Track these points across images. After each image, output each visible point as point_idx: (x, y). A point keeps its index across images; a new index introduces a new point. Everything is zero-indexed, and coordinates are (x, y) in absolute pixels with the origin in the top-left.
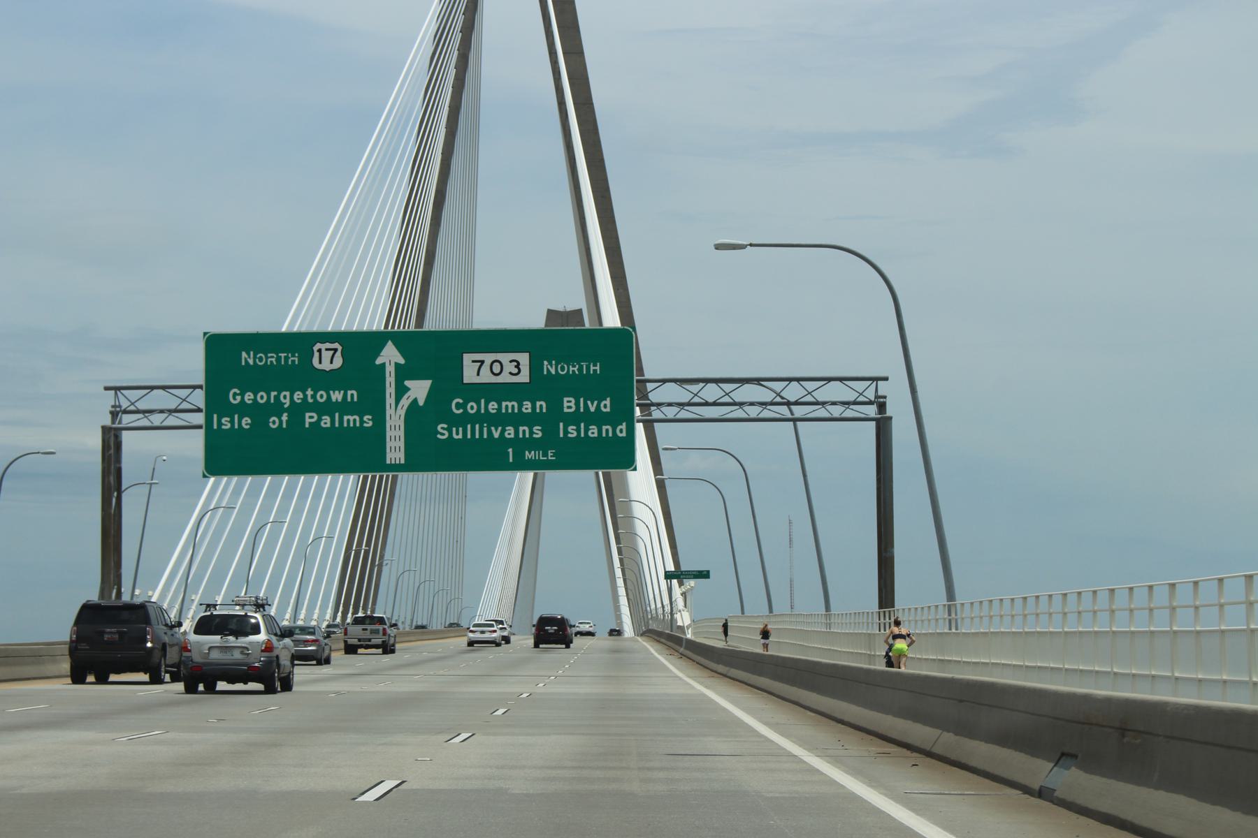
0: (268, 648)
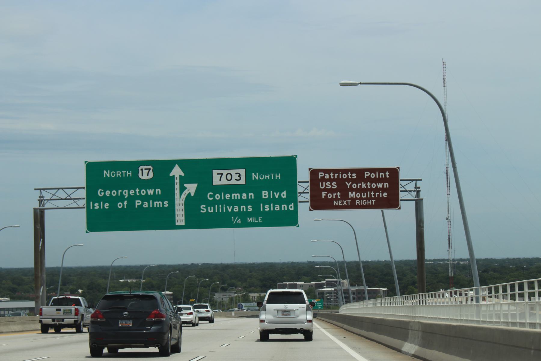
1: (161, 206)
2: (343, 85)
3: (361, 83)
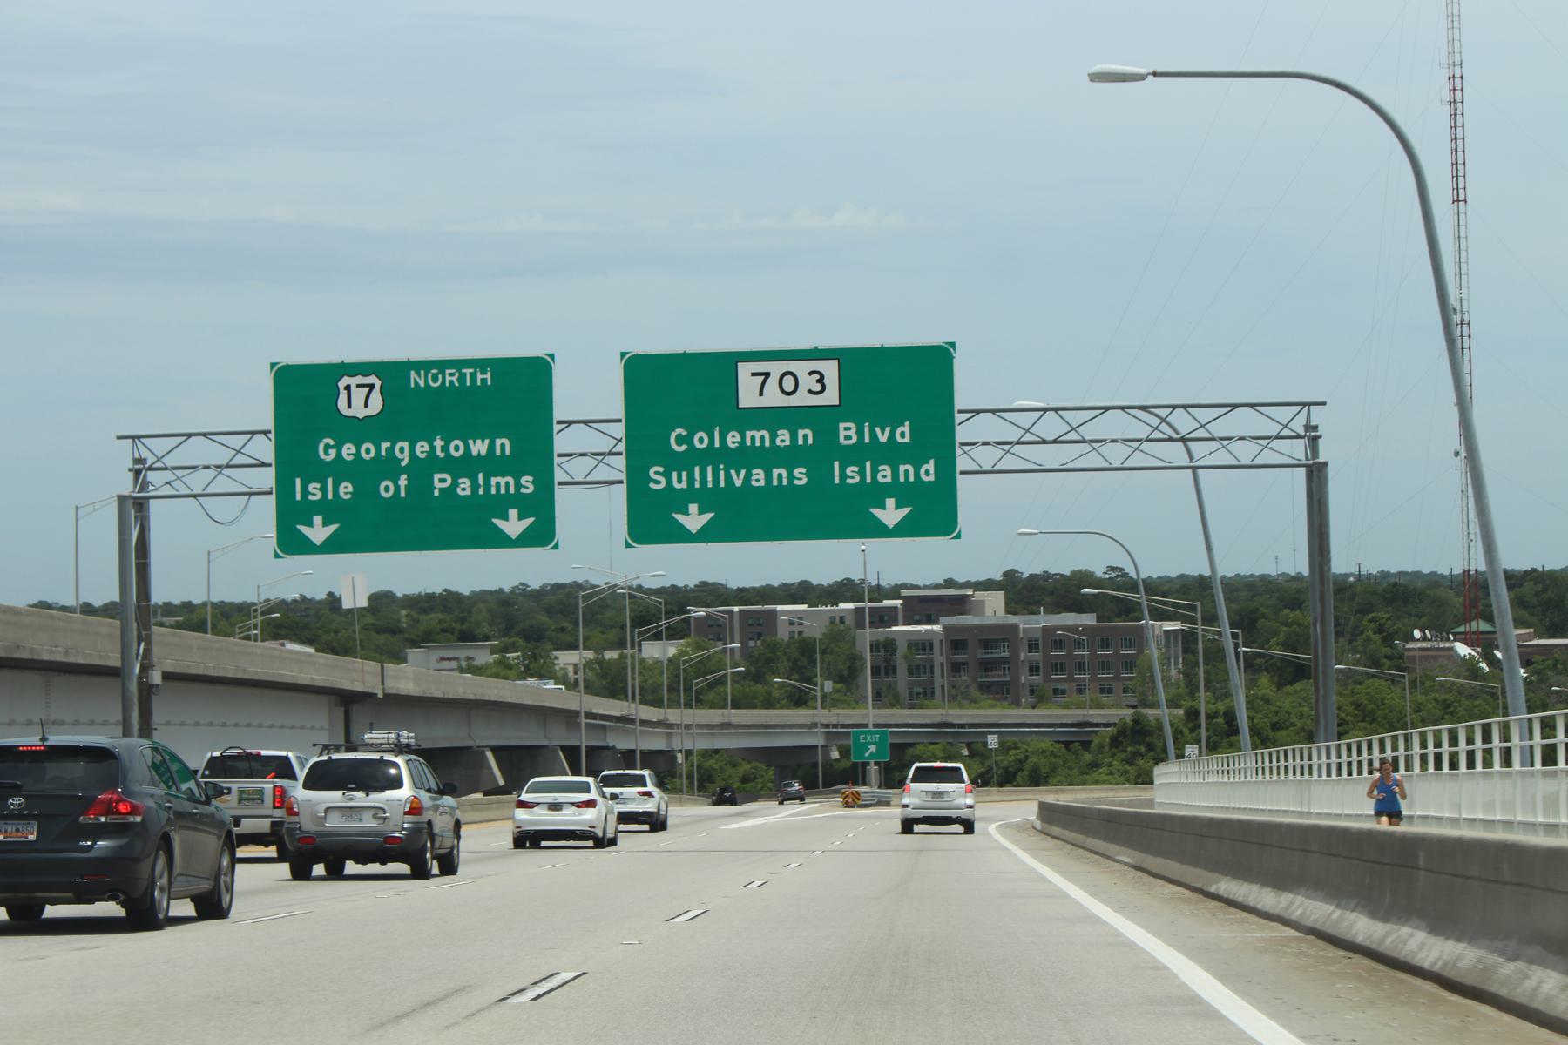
0: (415, 810)
1: (512, 491)
2: (1097, 77)
3: (1155, 74)
